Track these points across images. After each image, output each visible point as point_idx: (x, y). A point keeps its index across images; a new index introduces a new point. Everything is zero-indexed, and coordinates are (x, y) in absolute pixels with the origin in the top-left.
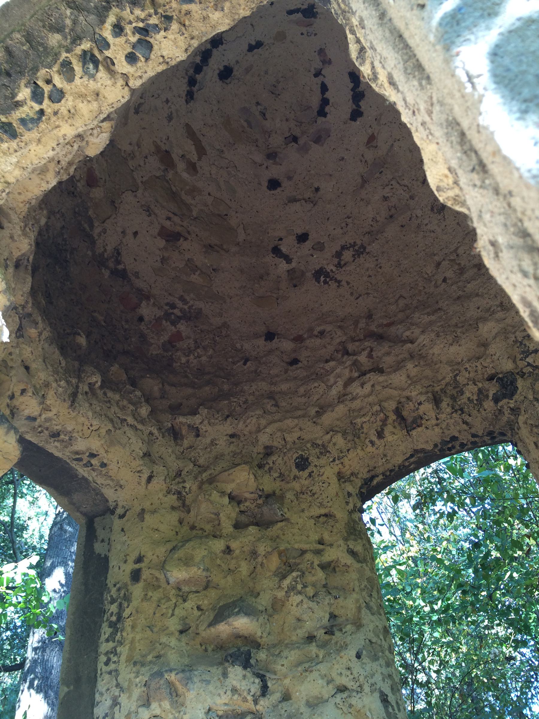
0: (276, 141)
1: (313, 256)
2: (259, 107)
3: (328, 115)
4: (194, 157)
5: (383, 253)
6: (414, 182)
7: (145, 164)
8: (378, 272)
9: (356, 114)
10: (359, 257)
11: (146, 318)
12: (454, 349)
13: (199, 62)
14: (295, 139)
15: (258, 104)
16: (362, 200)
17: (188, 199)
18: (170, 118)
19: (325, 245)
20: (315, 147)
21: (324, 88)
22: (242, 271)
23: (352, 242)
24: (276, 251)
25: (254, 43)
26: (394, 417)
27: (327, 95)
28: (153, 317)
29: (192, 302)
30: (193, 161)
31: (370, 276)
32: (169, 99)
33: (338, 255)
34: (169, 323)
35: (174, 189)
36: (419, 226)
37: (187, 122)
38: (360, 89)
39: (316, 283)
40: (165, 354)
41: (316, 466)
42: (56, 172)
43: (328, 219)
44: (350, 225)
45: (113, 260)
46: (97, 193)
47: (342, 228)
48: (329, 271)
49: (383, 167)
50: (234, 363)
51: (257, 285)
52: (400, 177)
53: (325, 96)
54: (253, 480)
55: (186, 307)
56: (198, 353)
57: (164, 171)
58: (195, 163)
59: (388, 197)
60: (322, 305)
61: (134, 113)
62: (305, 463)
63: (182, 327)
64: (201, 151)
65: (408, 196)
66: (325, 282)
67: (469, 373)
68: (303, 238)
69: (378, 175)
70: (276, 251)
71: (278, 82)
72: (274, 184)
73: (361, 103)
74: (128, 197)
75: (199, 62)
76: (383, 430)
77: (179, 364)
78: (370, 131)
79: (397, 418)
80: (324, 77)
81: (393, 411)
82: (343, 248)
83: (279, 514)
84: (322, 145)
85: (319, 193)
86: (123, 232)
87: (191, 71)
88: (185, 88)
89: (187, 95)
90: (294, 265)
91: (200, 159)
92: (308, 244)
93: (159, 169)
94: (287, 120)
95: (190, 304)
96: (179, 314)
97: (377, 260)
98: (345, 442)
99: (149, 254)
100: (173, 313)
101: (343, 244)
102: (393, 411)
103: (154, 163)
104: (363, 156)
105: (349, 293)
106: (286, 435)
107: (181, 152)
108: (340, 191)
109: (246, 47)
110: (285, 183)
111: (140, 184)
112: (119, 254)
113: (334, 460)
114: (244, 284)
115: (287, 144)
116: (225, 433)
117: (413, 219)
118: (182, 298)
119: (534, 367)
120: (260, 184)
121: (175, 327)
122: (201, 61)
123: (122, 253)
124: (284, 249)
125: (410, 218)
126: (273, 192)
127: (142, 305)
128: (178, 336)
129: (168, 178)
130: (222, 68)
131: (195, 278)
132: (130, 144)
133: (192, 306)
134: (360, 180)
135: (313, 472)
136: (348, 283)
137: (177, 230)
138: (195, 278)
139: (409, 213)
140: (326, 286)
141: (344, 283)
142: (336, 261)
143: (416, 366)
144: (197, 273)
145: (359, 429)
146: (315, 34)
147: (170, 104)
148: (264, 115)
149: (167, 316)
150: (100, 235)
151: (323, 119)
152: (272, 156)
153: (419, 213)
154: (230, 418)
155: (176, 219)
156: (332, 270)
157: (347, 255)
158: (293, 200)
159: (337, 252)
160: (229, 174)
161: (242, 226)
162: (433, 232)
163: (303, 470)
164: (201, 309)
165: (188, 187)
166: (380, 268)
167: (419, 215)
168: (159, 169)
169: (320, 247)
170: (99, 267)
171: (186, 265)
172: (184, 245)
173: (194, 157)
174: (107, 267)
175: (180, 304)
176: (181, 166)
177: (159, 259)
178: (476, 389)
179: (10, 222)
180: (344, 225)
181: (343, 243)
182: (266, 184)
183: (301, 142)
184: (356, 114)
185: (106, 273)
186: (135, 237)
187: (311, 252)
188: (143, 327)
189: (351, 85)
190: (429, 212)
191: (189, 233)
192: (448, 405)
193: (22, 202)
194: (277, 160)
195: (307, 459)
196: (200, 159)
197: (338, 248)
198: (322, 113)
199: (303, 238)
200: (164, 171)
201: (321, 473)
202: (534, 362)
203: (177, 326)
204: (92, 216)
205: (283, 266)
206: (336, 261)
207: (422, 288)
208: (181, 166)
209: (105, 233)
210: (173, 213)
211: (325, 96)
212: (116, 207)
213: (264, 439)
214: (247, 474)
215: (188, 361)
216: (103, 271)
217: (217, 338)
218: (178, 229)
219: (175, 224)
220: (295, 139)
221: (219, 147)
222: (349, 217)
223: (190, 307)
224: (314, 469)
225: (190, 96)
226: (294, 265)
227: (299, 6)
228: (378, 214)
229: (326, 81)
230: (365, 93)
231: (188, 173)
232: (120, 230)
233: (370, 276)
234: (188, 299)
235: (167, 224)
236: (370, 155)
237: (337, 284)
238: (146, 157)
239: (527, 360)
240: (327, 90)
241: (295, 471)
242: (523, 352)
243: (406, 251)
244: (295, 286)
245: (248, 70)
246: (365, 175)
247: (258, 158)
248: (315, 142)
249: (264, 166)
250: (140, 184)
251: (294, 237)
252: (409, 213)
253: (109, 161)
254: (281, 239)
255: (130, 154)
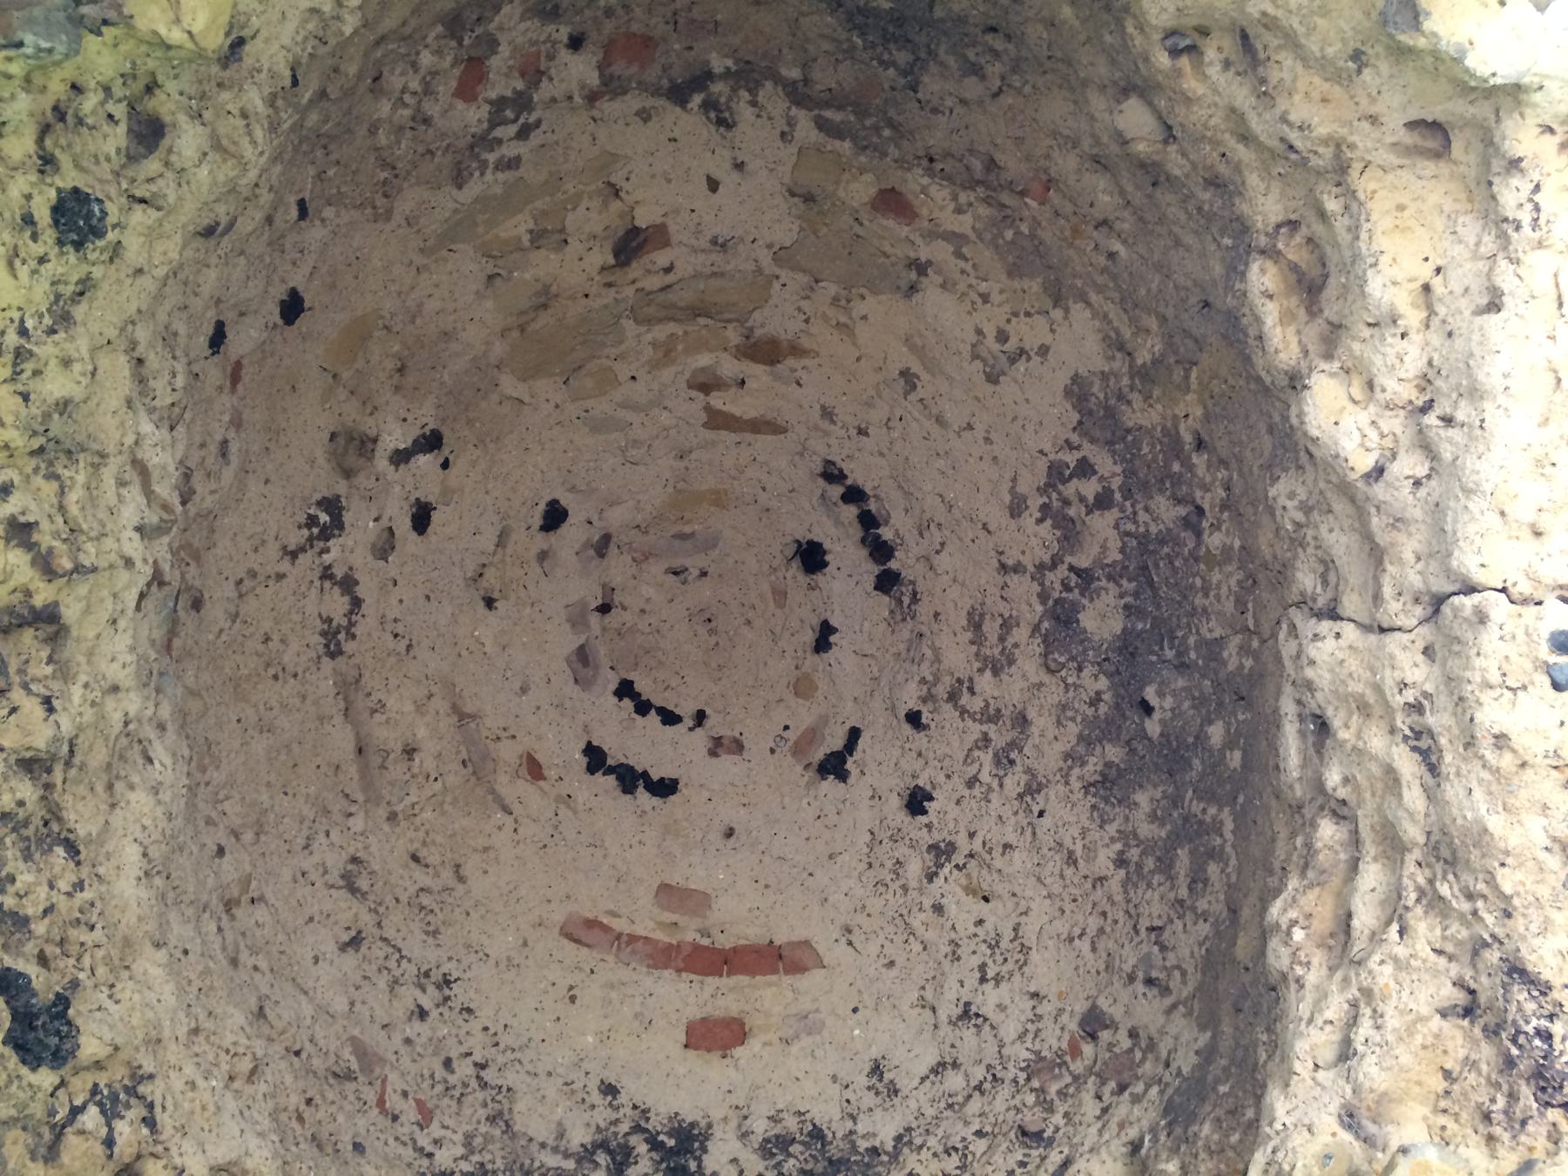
0: (618, 568)
1: (376, 520)
2: (696, 572)
3: (615, 700)
4: (717, 400)
5: (304, 698)
6: (421, 834)
7: (799, 309)
8: (268, 665)
9: (595, 758)
10: (324, 634)
11: (565, 55)
12: (132, 853)
13: (879, 531)
14: (604, 609)
15: (704, 574)
16: (430, 696)
17: (661, 332)
18: (828, 414)
19: (382, 563)
20: (572, 642)
21: (670, 718)
22: (446, 335)
23: (357, 630)
24: (431, 442)
25: (832, 639)
26: (38, 601)
27: (653, 718)
28: (553, 72)
29: (489, 177)
30: (714, 394)
31: (267, 639)
32: (865, 438)
33: (348, 584)
34: (509, 93)
35: (702, 321)
36: (327, 812)
37: (789, 434)
38: (641, 789)
39: (318, 496)
40: (479, 31)
41: (42, 260)
42: (1400, 316)
43: (428, 598)
44: (390, 643)
45: (723, 100)
46: (860, 190)
47: (395, 620)
48: (331, 543)
49: (474, 773)
50: (320, 176)
51: (396, 348)
52: (442, 804)
53: (653, 712)
54: (163, 31)
55: (491, 158)
56: (406, 105)
57: (751, 329)
58: (707, 394)
59: (411, 759)
60: (267, 481)
61: (908, 369)
62: (79, 230)
63: (474, 116)
64: (718, 420)
65: (399, 808)
66: (312, 521)
67: (69, 894)
68: (422, 518)
69: (464, 755)
70: (431, 442)
71: (712, 632)
72: (555, 517)
73: (611, 780)
74: (785, 233)
75: (879, 531)
76: (29, 546)
77: (429, 40)
78: (552, 774)
79: (32, 609)
80: (691, 729)
81: (56, 604)
82: (357, 603)
83: (29, 39)
84: (568, 661)
85: (482, 604)
86: (739, 166)
87: (873, 506)
88: (857, 475)
89: (841, 471)
90: (382, 463)
91: (708, 409)
92: (403, 525)
93: (763, 325)
94: (643, 611)
95: (489, 171)
96: (498, 132)
97: (295, 676)
98: (51, 401)
99: (653, 176)
100: (515, 120)
101: (364, 606)
102: (56, 604)
103: (776, 320)
104: (514, 737)
105: (257, 567)
106: (154, 214)
107: (750, 384)
108: (464, 653)
109: (834, 622)
110: (541, 541)
111: (777, 271)
112: (721, 122)
113: (23, 332)
114: (418, 321)
115: (604, 586)
116: (263, 34)
117: (345, 803)
118: (513, 163)
119: (64, 1127)
120: (573, 489)
121: (491, 102)
122: (879, 536)
123: (713, 128)
124: (424, 461)
125: (347, 796)
126: (542, 506)
127: (596, 74)
128: (467, 91)
129: (730, 327)
130: (827, 558)
131: (519, 226)
132: (864, 318)
133: (482, 174)
134: (469, 709)
135: (35, 237)
136: (280, 577)
137: (634, 264)
138: (519, 226)
139: (360, 797)
140: (302, 519)
141: (285, 566)
142: (339, 572)
143: (126, 724)
144: (526, 239)
145: (51, 464)
146: (772, 751)
147: (854, 432)
148: (676, 573)
149: (522, 102)
150: (791, 123)
151: (613, 686)
152: (603, 545)
153: (357, 824)
154: (288, 82)
155: (654, 282)
156: (327, 550)
157: (337, 605)
158: (502, 539)
159: (357, 583)
160: (635, 441)
161: (527, 399)
162: (306, 847)
163: (58, 210)
164: (460, 187)
165: (680, 347)
166: (276, 677)
167: (351, 822)
168: (763, 325)
169: (385, 547)
170: (748, 62)
171: (562, 230)
172: (603, 256)
173: (717, 400)
174: (728, 73)
175: (509, 150)
176: (730, 367)
177: (626, 186)
178: (30, 911)
179: (1394, 144)
180: (400, 629)
181: (365, 608)
182: (563, 502)
183: (595, 619)
184: (595, 758)
185: (718, 64)
186: (709, 178)
187: (384, 522)
188: (563, 33)
189: (655, 776)
190: (351, 850)
191: (609, 285)
192: (21, 803)
193: (1374, 192)
194: (592, 552)
195: (79, 245)
196: (708, 409)
197: (360, 591)
198: (625, 690)
199: (422, 518)
200: (751, 329)
201: (17, 263)
202: (82, 1132)
203: (487, 107)
204: (837, 143)
205: (395, 437)
206: (339, 572)
207: (207, 777)
208: (730, 367)
209: (783, 134)
210: (669, 286)
211: (653, 712)
212: (793, 194)
213: (188, 140)
214: (195, 30)
215: (415, 66)
216: (729, 63)
217: (385, 174)
218: (635, 270)
219: (649, 271)
220: (604, 609)
221: (693, 456)
222: (409, 647)
223: (484, 165)
224: (38, 249)
225: (831, 474)
226: (382, 463)
227: (857, 755)
228: (387, 721)
229: (680, 729)
230: (629, 796)
231: (703, 370)
232: (751, 166)
233: (267, 639)
234: (501, 176)
235: (662, 258)
236: (509, 753)
237: (292, 547)
238: (807, 321)
239: (93, 1110)
240: (664, 723)
241: (69, 178)
242: (114, 1098)
243: (283, 757)
244: (333, 436)
245: (780, 596)
246: (473, 725)
247: (617, 518)
248: (582, 648)
249: (595, 520)
250: (777, 271)
251: (431, 499)
252: (360, 797)
253: (882, 260)
254: (445, 465)
255: (849, 301)
